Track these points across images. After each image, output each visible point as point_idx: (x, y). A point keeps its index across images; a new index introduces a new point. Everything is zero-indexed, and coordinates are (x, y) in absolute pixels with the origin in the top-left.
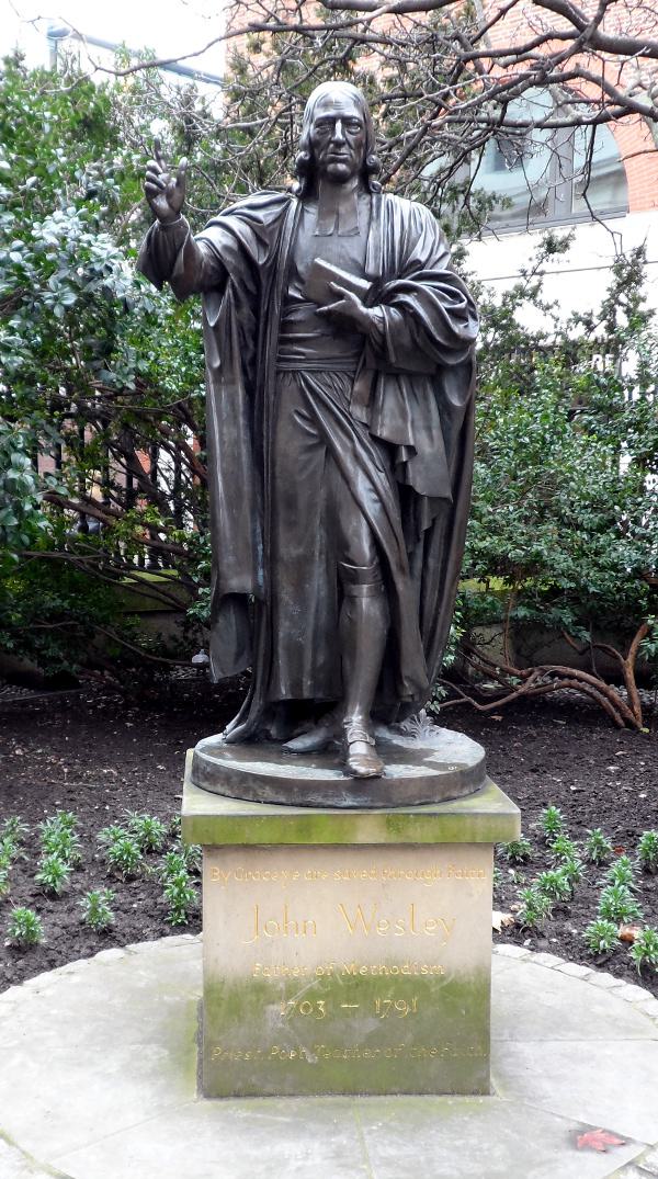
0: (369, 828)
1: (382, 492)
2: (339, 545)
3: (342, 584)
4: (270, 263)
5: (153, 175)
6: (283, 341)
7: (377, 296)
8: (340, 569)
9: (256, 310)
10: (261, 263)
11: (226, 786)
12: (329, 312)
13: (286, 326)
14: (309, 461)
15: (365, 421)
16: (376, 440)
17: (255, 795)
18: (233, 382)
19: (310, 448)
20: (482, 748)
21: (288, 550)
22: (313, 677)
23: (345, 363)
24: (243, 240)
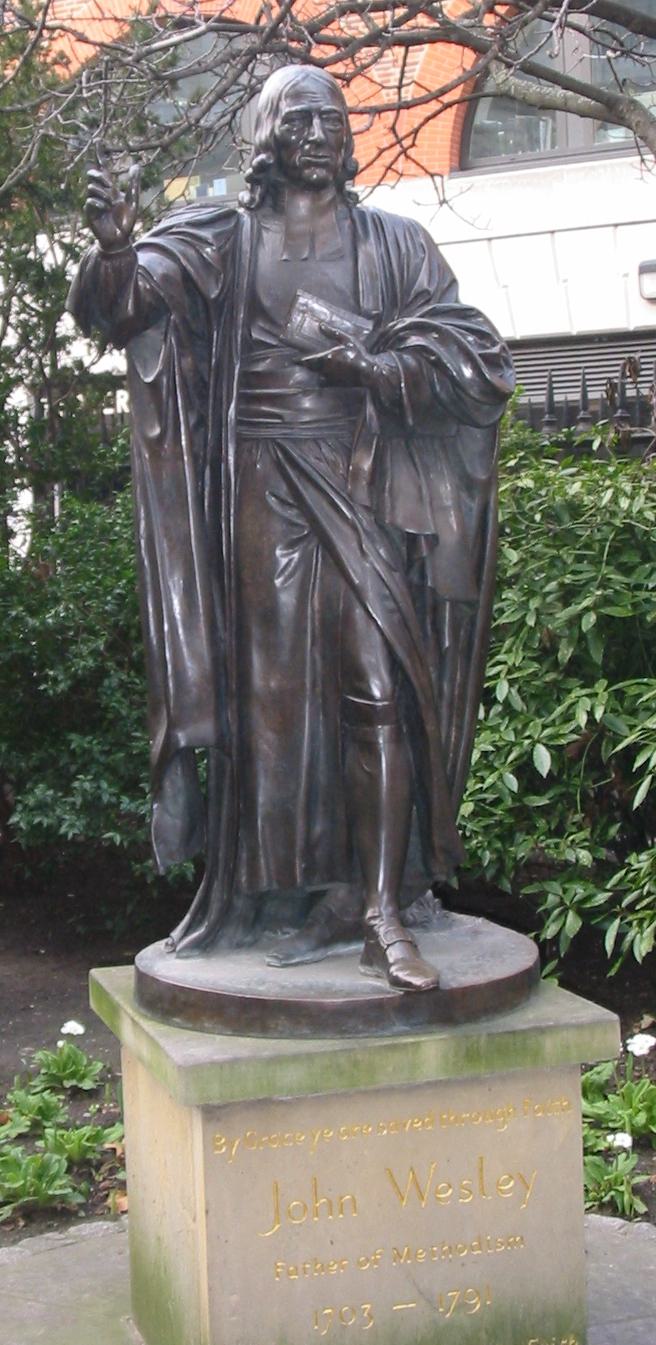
0: (432, 1049)
1: (399, 598)
3: (351, 721)
4: (222, 296)
5: (99, 189)
7: (382, 341)
10: (213, 296)
15: (367, 504)
16: (384, 530)
20: (454, 985)
23: (320, 428)
24: (189, 268)
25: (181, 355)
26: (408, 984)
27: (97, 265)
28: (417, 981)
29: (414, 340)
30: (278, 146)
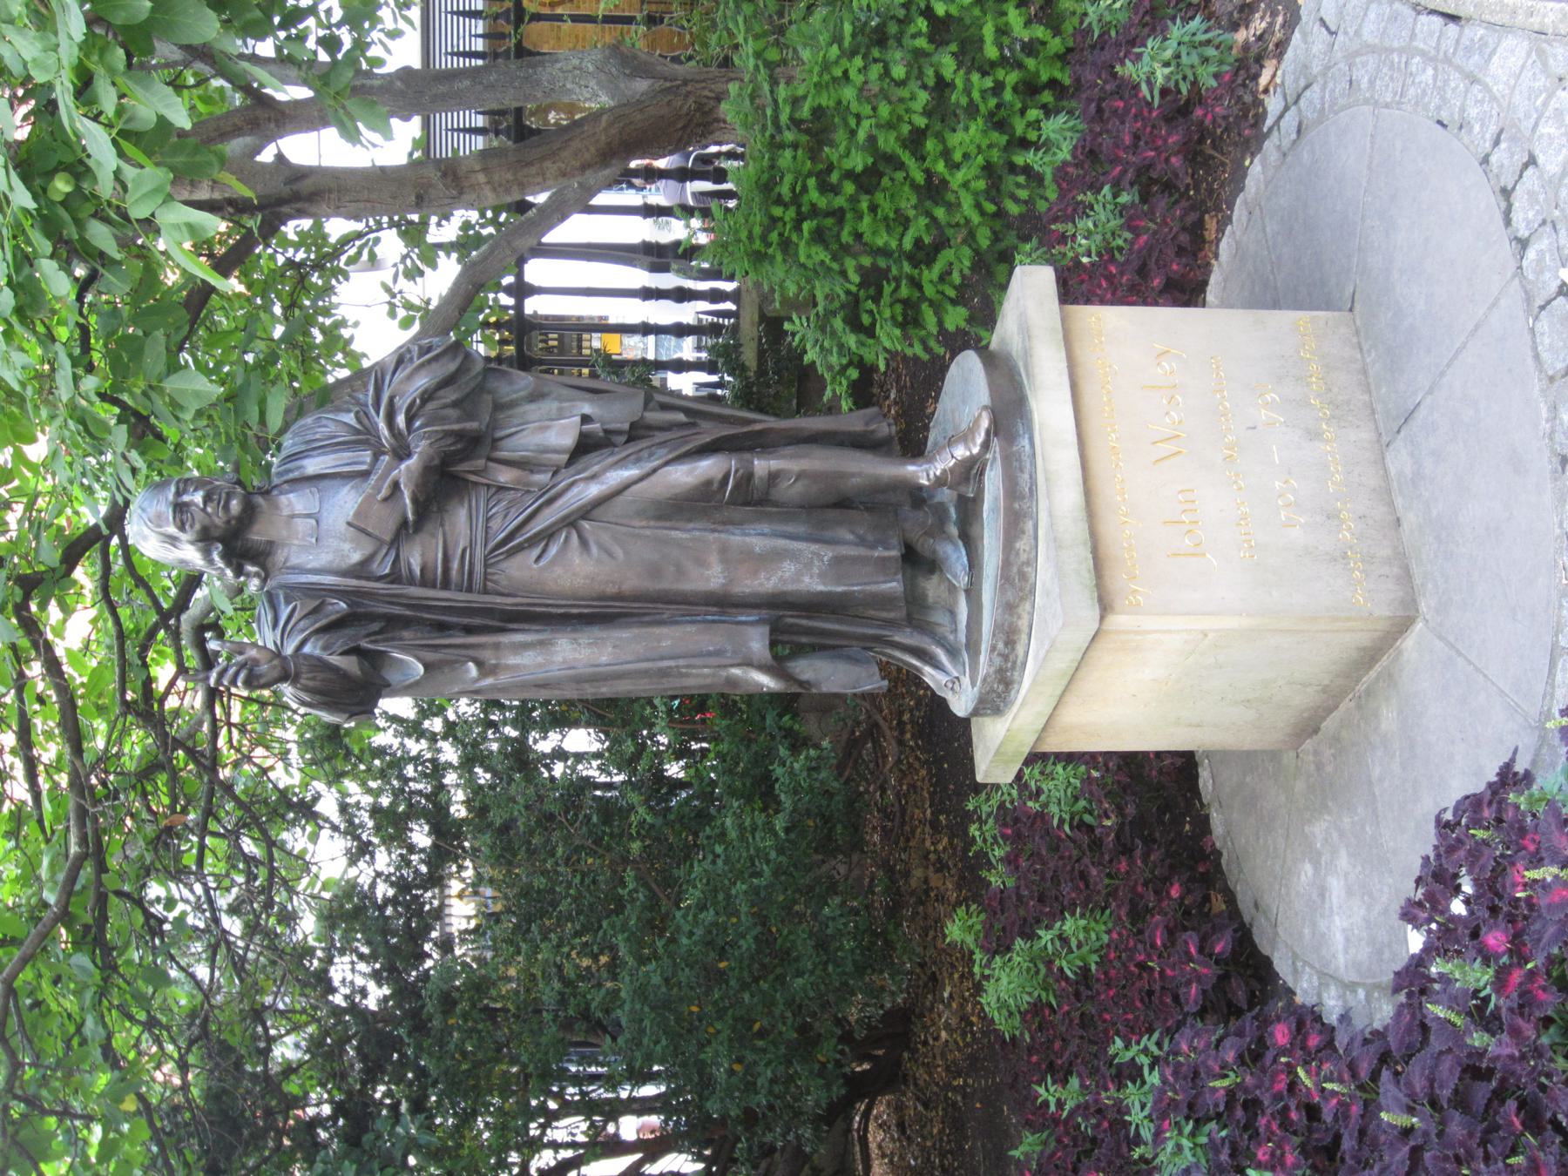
2: (698, 504)
6: (446, 585)
8: (733, 502)
9: (406, 623)
11: (1020, 610)
12: (415, 500)
13: (426, 581)
14: (601, 546)
17: (1028, 563)
18: (497, 646)
19: (584, 543)
21: (712, 577)
22: (873, 547)
25: (401, 639)
26: (988, 433)
27: (306, 689)
28: (985, 423)
29: (401, 420)
30: (205, 539)
